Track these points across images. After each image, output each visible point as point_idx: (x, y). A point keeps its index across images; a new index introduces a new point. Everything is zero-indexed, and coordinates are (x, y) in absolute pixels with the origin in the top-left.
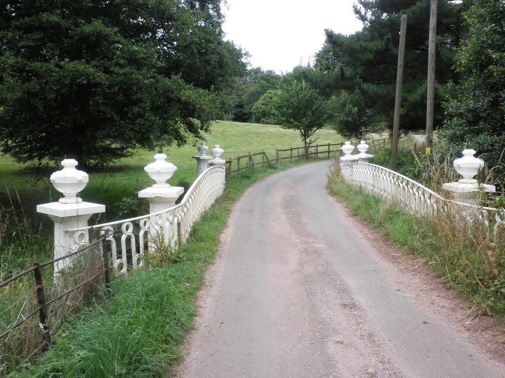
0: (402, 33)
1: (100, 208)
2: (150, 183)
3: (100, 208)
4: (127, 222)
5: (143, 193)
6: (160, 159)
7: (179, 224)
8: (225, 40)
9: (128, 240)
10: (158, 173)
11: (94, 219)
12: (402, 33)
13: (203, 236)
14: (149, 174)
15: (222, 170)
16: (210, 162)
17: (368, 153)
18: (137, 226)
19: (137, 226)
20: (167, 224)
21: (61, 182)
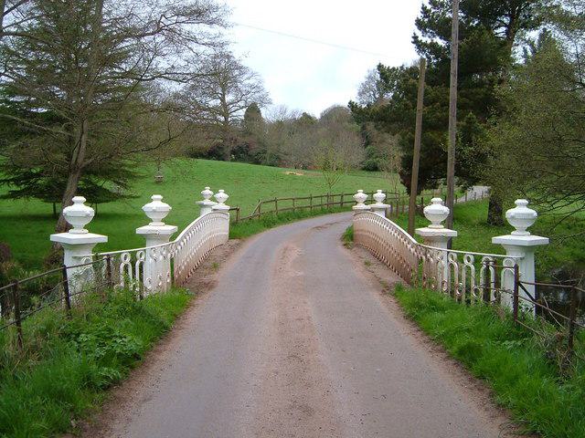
0: (454, 67)
1: (103, 238)
2: (147, 221)
3: (103, 238)
4: (125, 252)
5: (141, 230)
6: (158, 199)
7: (172, 260)
8: (318, 116)
9: (126, 266)
10: (154, 211)
11: (100, 247)
12: (454, 67)
13: (190, 284)
14: (147, 214)
15: (225, 216)
16: (213, 207)
17: (533, 233)
18: (133, 254)
19: (133, 254)
20: (161, 257)
21: (201, 161)
